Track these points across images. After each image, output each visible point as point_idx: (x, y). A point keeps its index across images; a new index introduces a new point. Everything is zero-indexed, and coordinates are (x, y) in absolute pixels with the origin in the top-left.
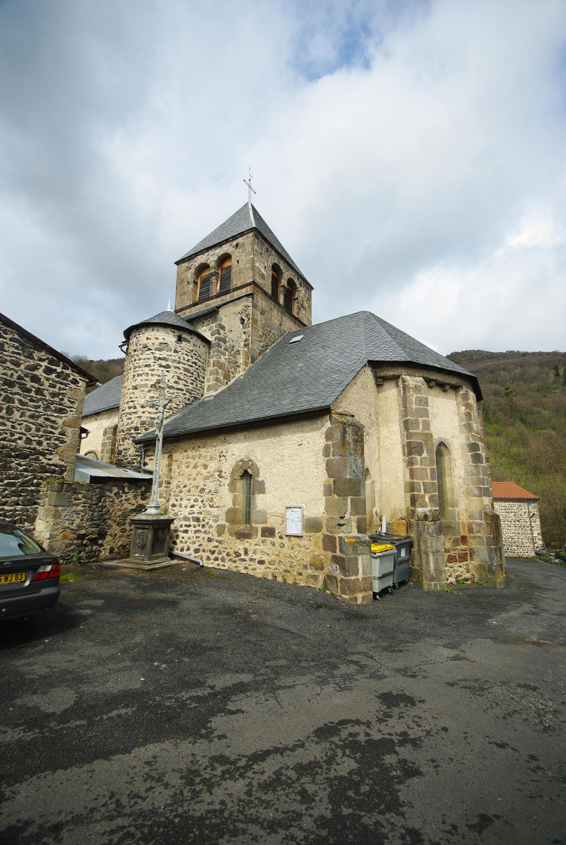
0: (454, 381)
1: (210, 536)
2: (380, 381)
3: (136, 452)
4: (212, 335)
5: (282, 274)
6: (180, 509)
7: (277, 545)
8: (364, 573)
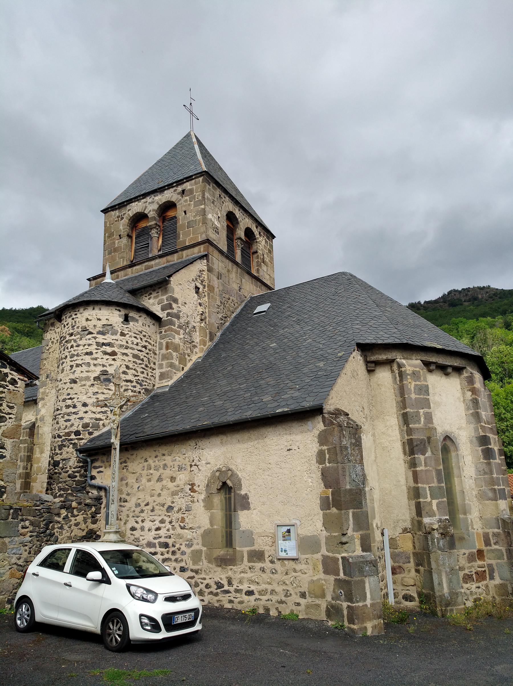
0: (457, 362)
1: (183, 564)
2: (372, 367)
3: (78, 462)
4: (163, 309)
5: (238, 223)
6: (142, 533)
7: (268, 571)
8: (372, 598)
